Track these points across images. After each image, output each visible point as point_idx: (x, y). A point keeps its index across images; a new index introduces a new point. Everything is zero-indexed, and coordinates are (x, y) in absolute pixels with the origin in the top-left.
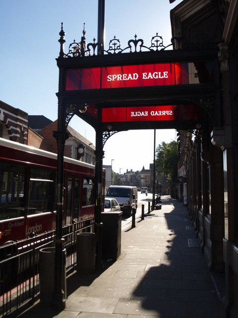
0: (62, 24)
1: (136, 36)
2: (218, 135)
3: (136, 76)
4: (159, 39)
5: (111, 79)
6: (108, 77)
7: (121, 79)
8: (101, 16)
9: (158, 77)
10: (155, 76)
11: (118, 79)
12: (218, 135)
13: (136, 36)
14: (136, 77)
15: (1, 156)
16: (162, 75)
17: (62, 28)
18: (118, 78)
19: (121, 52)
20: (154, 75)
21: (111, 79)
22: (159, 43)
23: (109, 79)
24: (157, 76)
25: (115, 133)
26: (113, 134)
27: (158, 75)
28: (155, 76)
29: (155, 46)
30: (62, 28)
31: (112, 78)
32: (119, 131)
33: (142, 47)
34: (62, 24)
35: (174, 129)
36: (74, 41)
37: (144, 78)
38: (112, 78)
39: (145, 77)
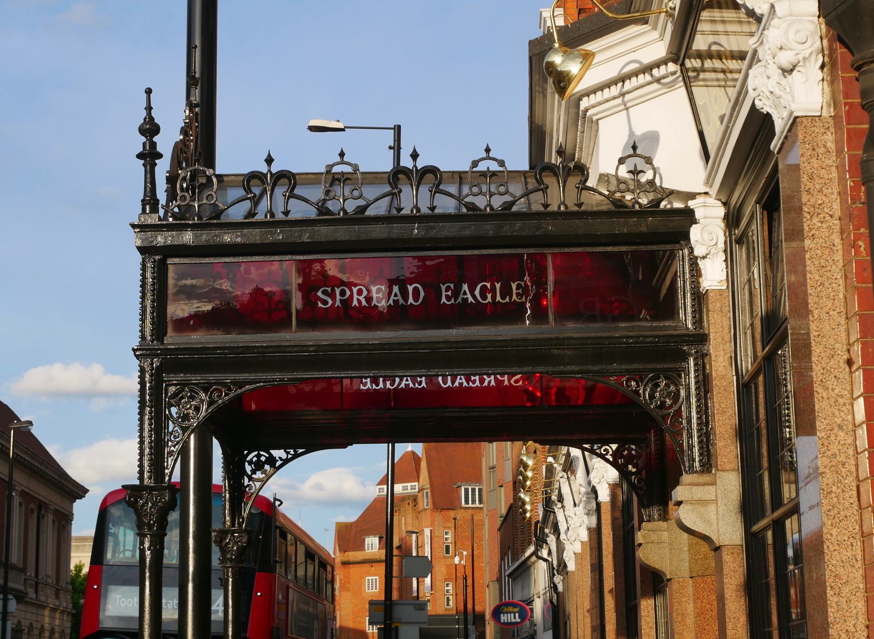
0: (149, 91)
1: (269, 161)
2: (716, 491)
3: (416, 291)
4: (641, 164)
5: (330, 302)
6: (320, 294)
7: (364, 303)
8: (692, 36)
9: (494, 297)
10: (484, 297)
11: (355, 303)
12: (716, 491)
13: (269, 161)
14: (416, 298)
15: (770, 634)
16: (506, 291)
17: (149, 108)
18: (355, 296)
19: (365, 208)
20: (477, 293)
21: (330, 302)
22: (643, 178)
23: (325, 302)
24: (489, 296)
25: (296, 456)
26: (286, 462)
27: (493, 290)
28: (484, 297)
29: (481, 193)
30: (149, 108)
31: (332, 296)
32: (311, 448)
33: (292, 200)
34: (149, 91)
35: (617, 473)
36: (342, 154)
37: (444, 300)
38: (334, 299)
39: (448, 298)
